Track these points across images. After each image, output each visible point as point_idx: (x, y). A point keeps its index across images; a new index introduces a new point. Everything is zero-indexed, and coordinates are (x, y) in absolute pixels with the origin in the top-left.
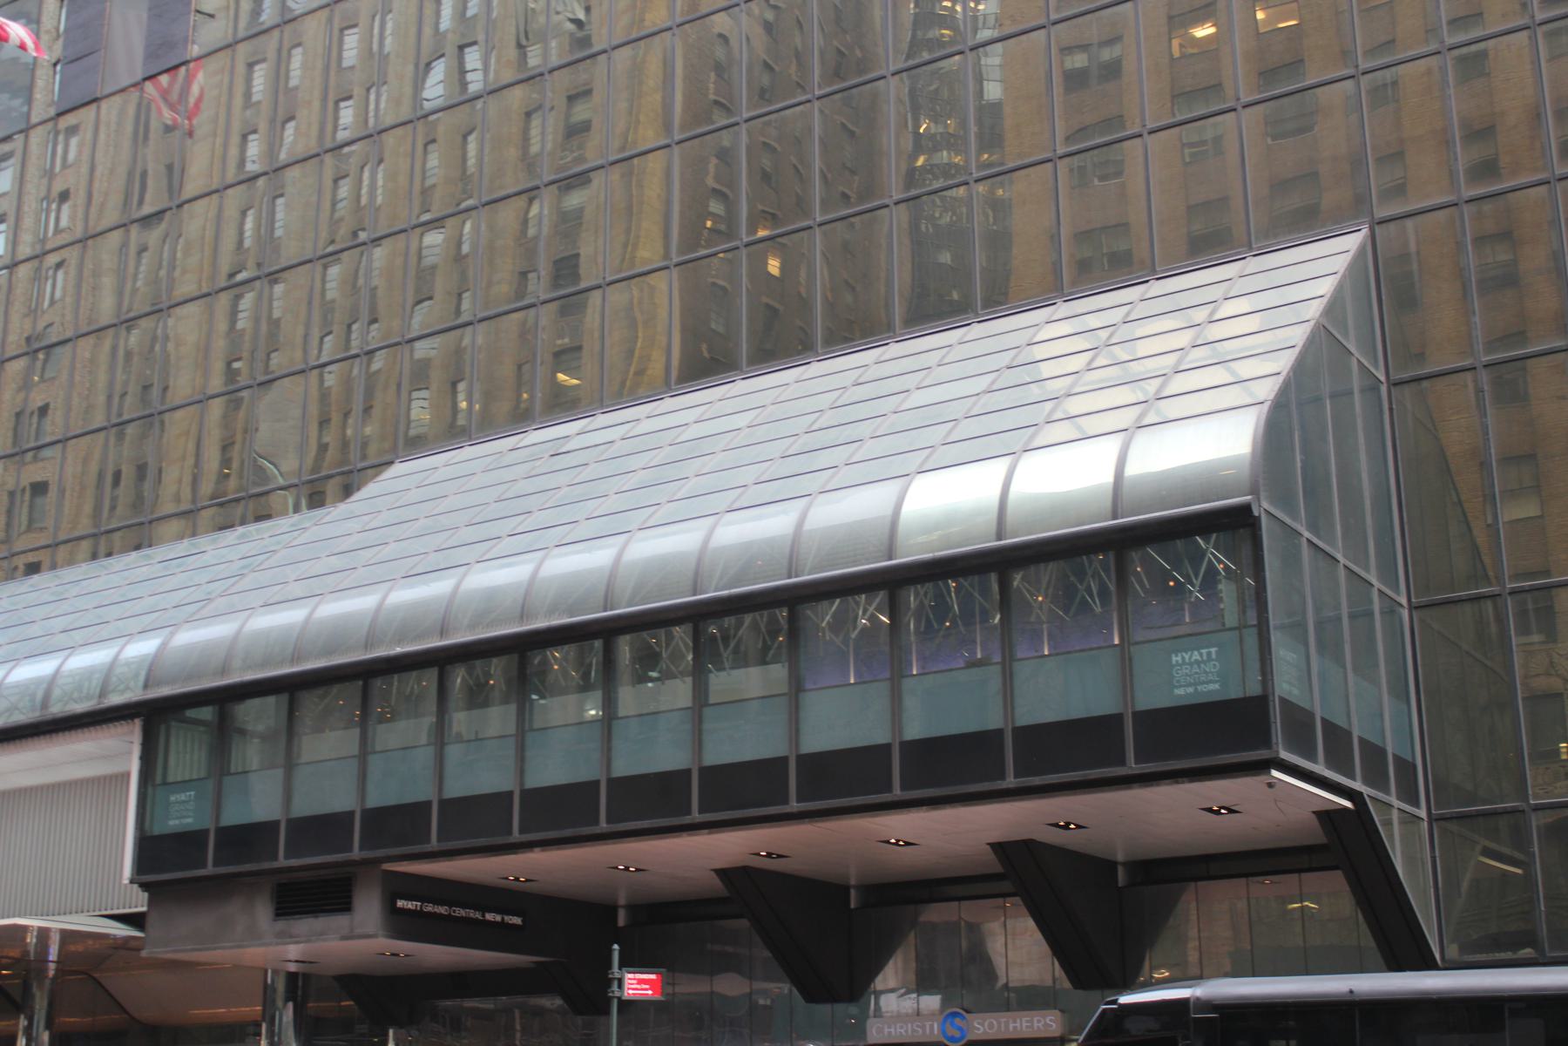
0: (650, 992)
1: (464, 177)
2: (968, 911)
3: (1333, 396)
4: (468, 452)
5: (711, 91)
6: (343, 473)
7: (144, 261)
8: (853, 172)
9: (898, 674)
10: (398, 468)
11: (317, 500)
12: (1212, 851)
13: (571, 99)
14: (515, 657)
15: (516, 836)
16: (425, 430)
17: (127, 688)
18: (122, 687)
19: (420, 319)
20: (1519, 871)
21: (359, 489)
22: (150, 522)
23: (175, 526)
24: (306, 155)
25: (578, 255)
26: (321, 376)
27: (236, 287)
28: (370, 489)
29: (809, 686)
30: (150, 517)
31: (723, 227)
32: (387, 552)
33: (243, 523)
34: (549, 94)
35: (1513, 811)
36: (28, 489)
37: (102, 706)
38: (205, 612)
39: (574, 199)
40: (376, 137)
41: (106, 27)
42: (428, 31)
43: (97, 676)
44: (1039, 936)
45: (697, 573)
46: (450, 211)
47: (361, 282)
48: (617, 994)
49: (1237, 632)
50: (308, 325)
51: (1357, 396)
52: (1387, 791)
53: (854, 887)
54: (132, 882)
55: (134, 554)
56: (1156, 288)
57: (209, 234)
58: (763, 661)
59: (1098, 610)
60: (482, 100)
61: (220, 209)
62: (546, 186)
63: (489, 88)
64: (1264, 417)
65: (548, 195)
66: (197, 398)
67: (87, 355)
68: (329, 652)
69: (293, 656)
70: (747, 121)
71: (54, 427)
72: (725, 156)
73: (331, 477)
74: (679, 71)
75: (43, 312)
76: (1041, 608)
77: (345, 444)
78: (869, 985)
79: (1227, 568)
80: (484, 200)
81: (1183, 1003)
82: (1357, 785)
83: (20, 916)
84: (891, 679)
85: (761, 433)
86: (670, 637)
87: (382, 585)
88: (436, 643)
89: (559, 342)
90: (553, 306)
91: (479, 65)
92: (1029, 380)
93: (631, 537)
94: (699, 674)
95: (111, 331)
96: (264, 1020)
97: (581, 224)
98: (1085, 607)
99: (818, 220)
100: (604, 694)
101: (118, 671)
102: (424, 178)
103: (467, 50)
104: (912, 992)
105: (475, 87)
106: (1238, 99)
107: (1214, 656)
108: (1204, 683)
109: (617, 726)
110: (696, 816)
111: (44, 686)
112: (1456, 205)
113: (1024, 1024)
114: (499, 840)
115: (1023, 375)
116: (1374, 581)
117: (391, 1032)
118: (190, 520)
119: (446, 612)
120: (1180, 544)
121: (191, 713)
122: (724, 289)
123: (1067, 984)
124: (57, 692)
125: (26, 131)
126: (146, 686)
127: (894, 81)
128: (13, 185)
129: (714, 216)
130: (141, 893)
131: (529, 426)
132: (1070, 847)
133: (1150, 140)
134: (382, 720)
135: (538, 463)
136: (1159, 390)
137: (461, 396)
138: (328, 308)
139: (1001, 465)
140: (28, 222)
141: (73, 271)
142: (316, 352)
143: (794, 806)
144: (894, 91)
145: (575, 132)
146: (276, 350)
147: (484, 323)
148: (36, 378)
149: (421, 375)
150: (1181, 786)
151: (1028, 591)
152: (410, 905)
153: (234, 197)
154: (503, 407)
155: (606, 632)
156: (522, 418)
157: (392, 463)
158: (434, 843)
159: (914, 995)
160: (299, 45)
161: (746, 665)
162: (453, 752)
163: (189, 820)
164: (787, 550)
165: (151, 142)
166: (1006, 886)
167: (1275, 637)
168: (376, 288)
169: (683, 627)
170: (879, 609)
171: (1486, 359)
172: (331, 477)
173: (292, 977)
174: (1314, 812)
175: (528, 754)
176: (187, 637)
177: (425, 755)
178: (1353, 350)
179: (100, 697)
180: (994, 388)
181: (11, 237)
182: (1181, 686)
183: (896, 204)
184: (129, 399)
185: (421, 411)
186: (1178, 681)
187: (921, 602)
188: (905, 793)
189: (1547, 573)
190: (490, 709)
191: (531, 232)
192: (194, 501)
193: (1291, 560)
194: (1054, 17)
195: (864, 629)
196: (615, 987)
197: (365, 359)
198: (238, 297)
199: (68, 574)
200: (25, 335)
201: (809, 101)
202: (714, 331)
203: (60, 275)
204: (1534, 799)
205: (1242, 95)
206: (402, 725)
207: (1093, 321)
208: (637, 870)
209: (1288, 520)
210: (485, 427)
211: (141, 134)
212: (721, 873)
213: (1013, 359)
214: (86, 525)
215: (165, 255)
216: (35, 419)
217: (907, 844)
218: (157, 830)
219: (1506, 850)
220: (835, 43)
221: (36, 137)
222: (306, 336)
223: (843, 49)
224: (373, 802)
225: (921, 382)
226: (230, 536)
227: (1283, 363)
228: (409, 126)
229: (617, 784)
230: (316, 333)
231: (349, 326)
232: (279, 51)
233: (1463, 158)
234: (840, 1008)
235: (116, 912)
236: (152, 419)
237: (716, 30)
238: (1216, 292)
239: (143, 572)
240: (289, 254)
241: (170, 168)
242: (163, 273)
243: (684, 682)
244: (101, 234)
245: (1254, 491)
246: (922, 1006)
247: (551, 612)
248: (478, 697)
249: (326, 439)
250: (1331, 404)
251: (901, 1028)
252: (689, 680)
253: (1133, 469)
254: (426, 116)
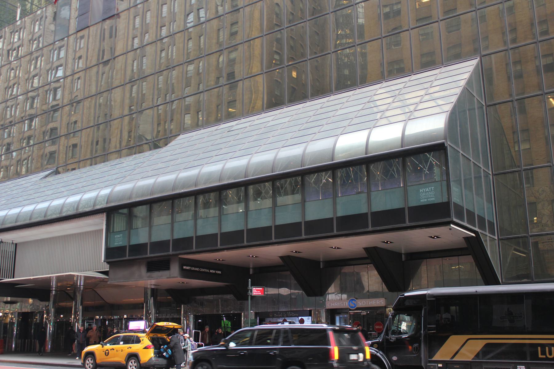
0: (260, 293)
2: (357, 269)
3: (469, 110)
4: (202, 131)
5: (274, 21)
6: (164, 138)
8: (318, 46)
9: (335, 196)
10: (181, 137)
11: (156, 146)
12: (431, 250)
13: (232, 25)
14: (218, 193)
15: (219, 247)
18: (100, 204)
19: (188, 91)
20: (525, 255)
21: (170, 143)
24: (152, 42)
25: (234, 72)
26: (158, 109)
27: (132, 82)
28: (173, 143)
29: (307, 200)
30: (107, 153)
31: (278, 63)
33: (135, 154)
35: (525, 237)
36: (71, 146)
37: (94, 209)
38: (124, 181)
39: (233, 55)
40: (173, 36)
41: (91, 5)
42: (188, 5)
43: (92, 200)
45: (273, 166)
47: (169, 82)
48: (250, 294)
49: (440, 182)
51: (476, 110)
52: (486, 231)
53: (322, 262)
54: (104, 262)
55: (103, 164)
57: (123, 67)
58: (293, 193)
59: (396, 176)
60: (205, 23)
61: (126, 58)
62: (225, 49)
65: (226, 52)
66: (120, 117)
67: (88, 105)
71: (79, 126)
74: (265, 13)
75: (74, 93)
76: (378, 176)
77: (165, 130)
79: (436, 163)
81: (425, 295)
82: (476, 229)
83: (72, 272)
84: (333, 198)
85: (292, 123)
86: (265, 186)
87: (177, 172)
89: (229, 99)
90: (227, 86)
91: (204, 16)
92: (373, 106)
93: (253, 156)
94: (274, 198)
96: (145, 303)
97: (235, 63)
98: (392, 176)
99: (309, 58)
101: (99, 199)
102: (188, 50)
103: (200, 10)
105: (202, 20)
106: (439, 18)
109: (249, 213)
110: (274, 240)
111: (77, 204)
112: (507, 50)
116: (482, 167)
117: (182, 306)
118: (119, 153)
119: (196, 179)
121: (121, 211)
122: (280, 82)
123: (387, 290)
124: (81, 206)
126: (107, 203)
127: (331, 15)
128: (64, 55)
129: (276, 60)
130: (107, 265)
131: (221, 123)
132: (388, 249)
134: (178, 213)
135: (224, 134)
137: (200, 116)
140: (70, 66)
141: (83, 80)
142: (156, 102)
143: (304, 237)
144: (331, 18)
145: (233, 34)
146: (144, 102)
148: (73, 113)
149: (187, 110)
150: (423, 230)
151: (374, 170)
152: (188, 268)
153: (131, 55)
154: (213, 118)
155: (245, 185)
156: (218, 121)
157: (180, 135)
158: (194, 249)
160: (149, 10)
162: (200, 222)
163: (121, 243)
164: (301, 159)
165: (106, 41)
166: (368, 261)
167: (452, 184)
168: (174, 83)
169: (269, 183)
170: (329, 177)
171: (516, 98)
173: (153, 290)
174: (463, 238)
175: (222, 223)
177: (191, 223)
178: (475, 95)
179: (93, 206)
180: (364, 108)
181: (64, 71)
182: (423, 199)
183: (332, 53)
184: (100, 118)
185: (188, 120)
186: (422, 197)
187: (342, 175)
188: (338, 232)
189: (532, 165)
190: (210, 209)
191: (220, 66)
192: (120, 147)
193: (457, 161)
195: (324, 183)
197: (171, 103)
198: (132, 86)
199: (83, 170)
200: (69, 99)
201: (305, 21)
202: (277, 95)
203: (79, 81)
204: (531, 233)
206: (184, 214)
207: (393, 88)
208: (256, 257)
209: (456, 148)
210: (207, 124)
212: (281, 257)
213: (369, 100)
216: (73, 125)
217: (338, 248)
218: (112, 246)
219: (521, 249)
220: (313, 6)
221: (72, 38)
222: (153, 99)
223: (315, 7)
224: (176, 237)
225: (341, 107)
226: (131, 158)
228: (183, 32)
229: (250, 231)
230: (156, 97)
231: (166, 95)
232: (143, 12)
233: (509, 37)
234: (317, 298)
235: (100, 270)
236: (107, 123)
238: (432, 78)
239: (106, 169)
240: (148, 72)
241: (111, 48)
242: (110, 80)
243: (269, 200)
244: (91, 67)
248: (206, 205)
249: (159, 129)
250: (469, 112)
251: (336, 304)
252: (271, 199)
253: (407, 133)
254: (188, 29)
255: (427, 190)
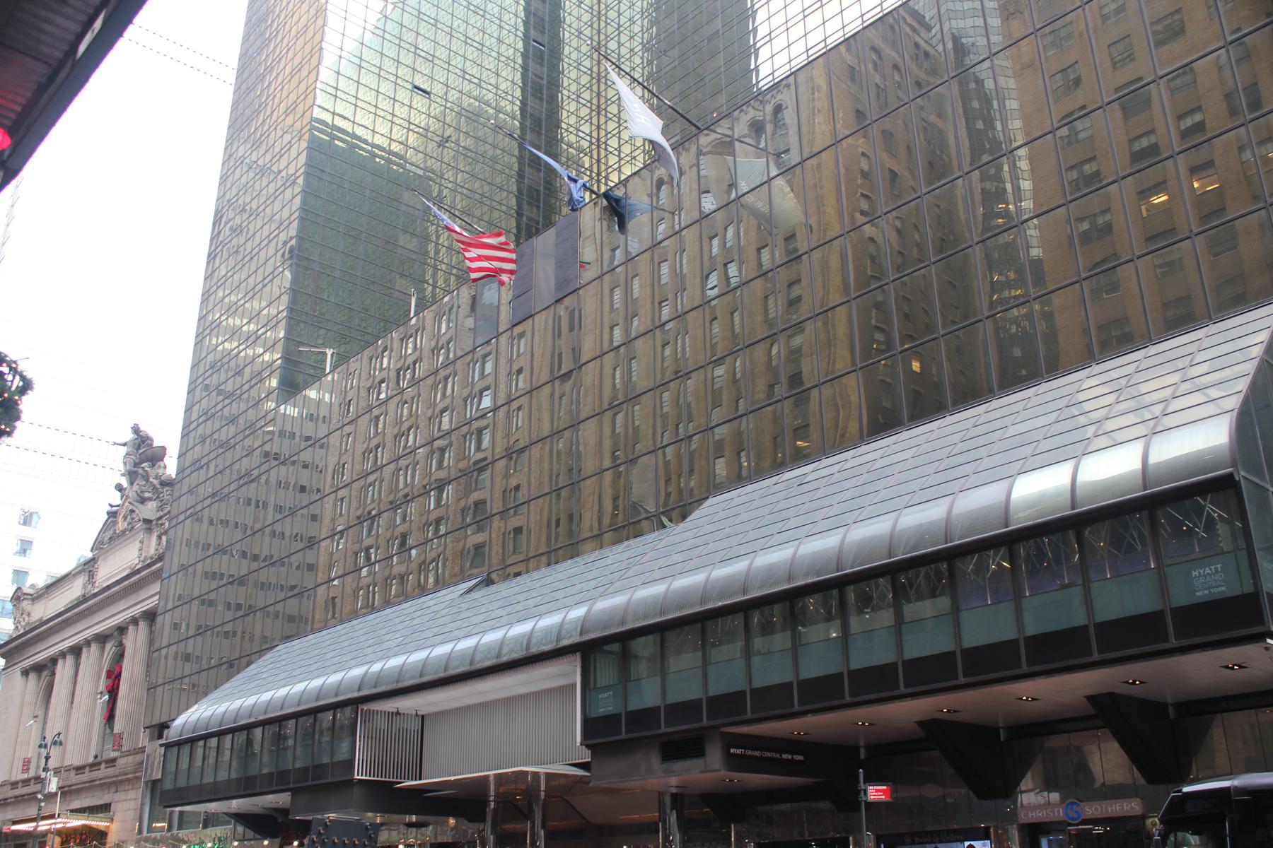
1: (734, 336)
2: (1075, 739)
4: (750, 488)
6: (681, 506)
7: (563, 402)
8: (957, 308)
9: (1018, 596)
10: (711, 501)
12: (1230, 693)
13: (790, 285)
15: (797, 708)
16: (724, 480)
17: (571, 636)
19: (717, 415)
21: (690, 514)
22: (577, 543)
23: (589, 545)
25: (801, 372)
26: (664, 454)
28: (697, 514)
31: (883, 347)
32: (710, 547)
33: (627, 539)
34: (778, 286)
36: (512, 532)
38: (611, 590)
39: (796, 341)
43: (554, 630)
44: (1122, 752)
45: (890, 546)
46: (727, 353)
47: (682, 400)
48: (864, 799)
49: (1233, 554)
50: (654, 426)
56: (1153, 350)
58: (933, 595)
59: (1140, 548)
63: (744, 281)
64: (1234, 419)
65: (782, 338)
68: (681, 607)
69: (838, 566)
70: (893, 281)
72: (881, 307)
73: (674, 509)
78: (1016, 788)
79: (1219, 516)
80: (747, 344)
81: (1227, 789)
85: (920, 461)
86: (877, 586)
88: (356, 695)
89: (796, 423)
90: (791, 400)
91: (736, 274)
95: (549, 439)
97: (801, 355)
100: (894, 610)
103: (729, 266)
104: (1045, 791)
106: (1191, 231)
107: (1219, 569)
108: (1214, 587)
111: (527, 638)
113: (1118, 808)
114: (787, 711)
115: (1075, 411)
118: (598, 540)
120: (1187, 503)
121: (607, 648)
123: (1143, 782)
124: (534, 641)
125: (497, 337)
126: (581, 634)
127: (977, 248)
129: (878, 342)
133: (1139, 263)
134: (714, 645)
135: (792, 490)
136: (1164, 410)
137: (743, 459)
138: (664, 417)
139: (1005, 484)
141: (526, 410)
144: (977, 254)
145: (794, 303)
147: (753, 414)
150: (1207, 653)
152: (738, 751)
155: (840, 583)
156: (778, 466)
157: (708, 498)
158: (749, 715)
159: (1046, 793)
160: (637, 275)
161: (924, 600)
162: (756, 661)
165: (563, 337)
172: (674, 509)
173: (674, 796)
176: (602, 605)
177: (740, 664)
182: (1199, 590)
184: (561, 478)
185: (721, 467)
187: (1028, 552)
191: (774, 363)
192: (600, 529)
194: (1069, 198)
196: (862, 795)
198: (615, 415)
199: (536, 575)
205: (1193, 228)
207: (1114, 374)
209: (1258, 482)
210: (758, 473)
211: (557, 333)
212: (920, 723)
214: (543, 548)
215: (574, 397)
216: (513, 493)
218: (594, 715)
224: (711, 693)
226: (620, 547)
227: (1243, 385)
230: (659, 431)
236: (574, 485)
237: (867, 235)
239: (575, 571)
240: (642, 386)
241: (573, 350)
242: (574, 407)
245: (1234, 465)
246: (1051, 799)
247: (807, 575)
248: (767, 629)
249: (669, 490)
252: (892, 609)
253: (1153, 459)
255: (1208, 571)
